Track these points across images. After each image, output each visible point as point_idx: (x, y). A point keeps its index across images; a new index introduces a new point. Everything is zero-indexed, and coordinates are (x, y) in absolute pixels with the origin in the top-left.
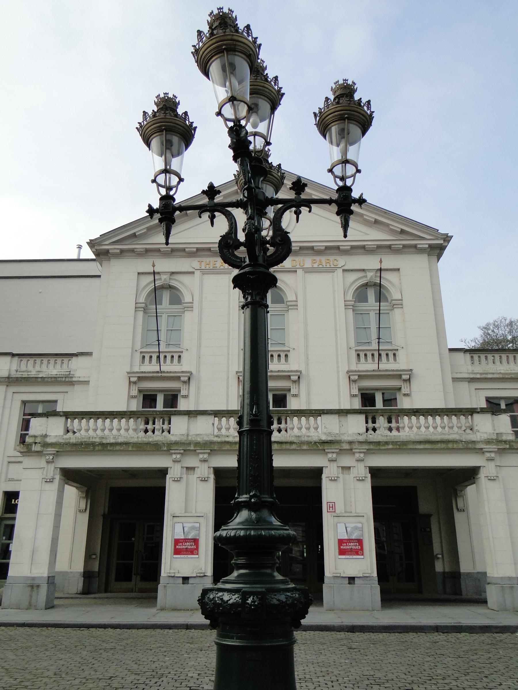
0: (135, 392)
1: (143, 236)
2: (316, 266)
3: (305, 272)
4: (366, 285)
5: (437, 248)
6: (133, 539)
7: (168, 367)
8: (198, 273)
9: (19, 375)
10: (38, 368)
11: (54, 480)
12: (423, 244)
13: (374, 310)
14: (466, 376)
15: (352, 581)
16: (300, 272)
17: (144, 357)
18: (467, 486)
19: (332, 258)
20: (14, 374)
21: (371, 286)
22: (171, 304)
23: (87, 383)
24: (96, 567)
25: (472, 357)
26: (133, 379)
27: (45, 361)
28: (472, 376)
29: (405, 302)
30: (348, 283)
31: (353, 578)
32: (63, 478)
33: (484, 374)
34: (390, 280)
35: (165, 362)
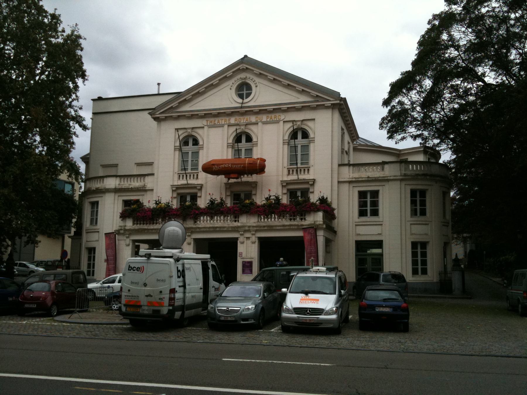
0: (175, 195)
1: (177, 107)
2: (268, 120)
3: (209, 127)
7: (302, 177)
8: (206, 128)
9: (120, 187)
10: (129, 182)
14: (347, 180)
16: (260, 124)
17: (179, 176)
19: (277, 115)
20: (118, 187)
22: (246, 142)
23: (152, 190)
26: (174, 189)
27: (136, 179)
28: (350, 180)
29: (316, 139)
30: (286, 129)
33: (395, 176)
34: (310, 127)
35: (300, 173)
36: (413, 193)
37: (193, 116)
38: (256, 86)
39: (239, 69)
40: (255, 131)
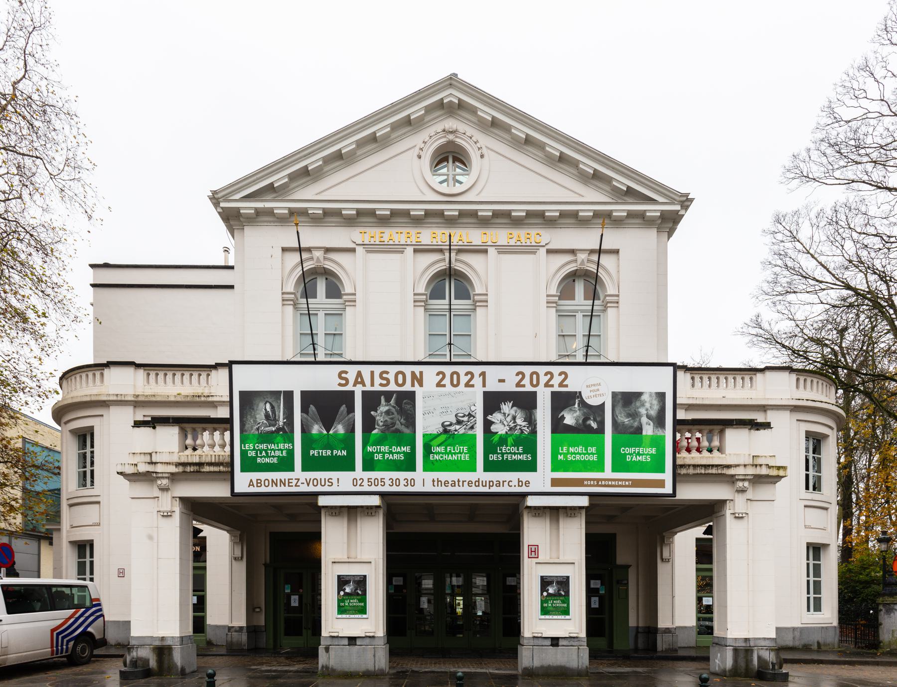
2: (512, 242)
3: (499, 253)
4: (573, 276)
5: (669, 222)
6: (405, 591)
11: (173, 514)
12: (654, 211)
13: (582, 311)
15: (555, 642)
18: (676, 533)
19: (533, 232)
21: (580, 276)
24: (261, 621)
25: (693, 378)
27: (170, 375)
31: (558, 639)
32: (184, 511)
36: (809, 435)
37: (330, 216)
38: (482, 156)
39: (440, 104)
40: (481, 271)
